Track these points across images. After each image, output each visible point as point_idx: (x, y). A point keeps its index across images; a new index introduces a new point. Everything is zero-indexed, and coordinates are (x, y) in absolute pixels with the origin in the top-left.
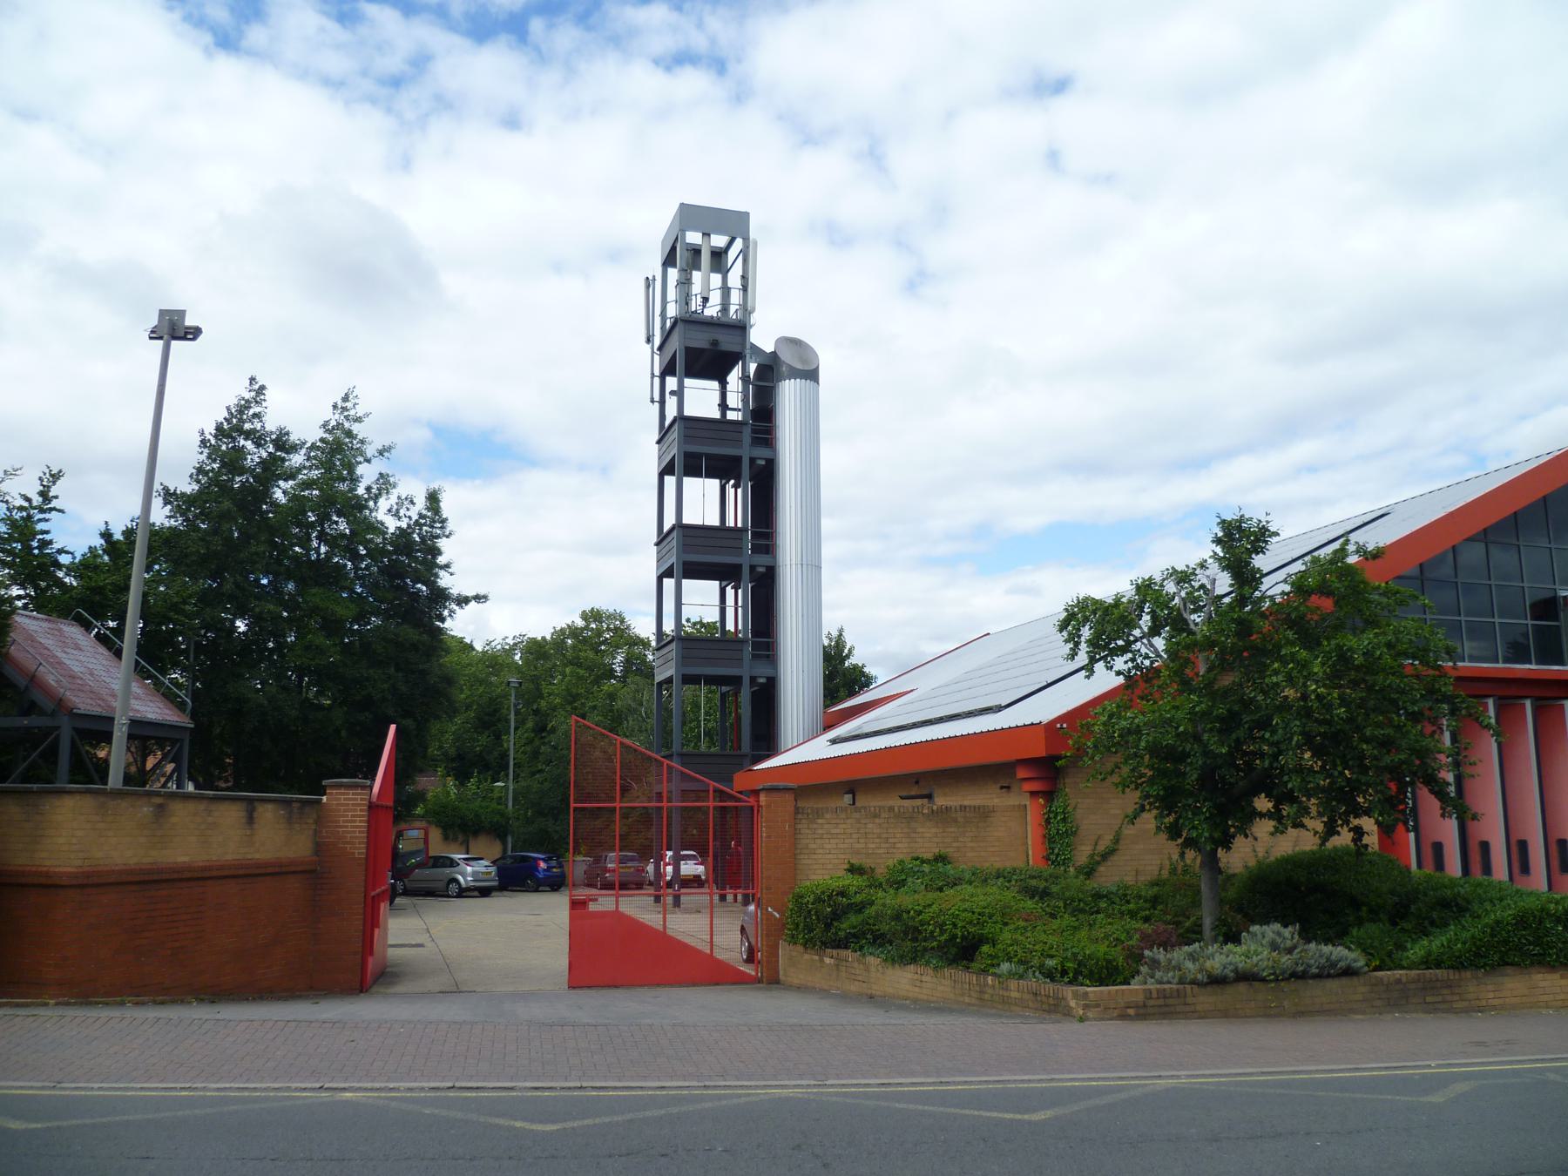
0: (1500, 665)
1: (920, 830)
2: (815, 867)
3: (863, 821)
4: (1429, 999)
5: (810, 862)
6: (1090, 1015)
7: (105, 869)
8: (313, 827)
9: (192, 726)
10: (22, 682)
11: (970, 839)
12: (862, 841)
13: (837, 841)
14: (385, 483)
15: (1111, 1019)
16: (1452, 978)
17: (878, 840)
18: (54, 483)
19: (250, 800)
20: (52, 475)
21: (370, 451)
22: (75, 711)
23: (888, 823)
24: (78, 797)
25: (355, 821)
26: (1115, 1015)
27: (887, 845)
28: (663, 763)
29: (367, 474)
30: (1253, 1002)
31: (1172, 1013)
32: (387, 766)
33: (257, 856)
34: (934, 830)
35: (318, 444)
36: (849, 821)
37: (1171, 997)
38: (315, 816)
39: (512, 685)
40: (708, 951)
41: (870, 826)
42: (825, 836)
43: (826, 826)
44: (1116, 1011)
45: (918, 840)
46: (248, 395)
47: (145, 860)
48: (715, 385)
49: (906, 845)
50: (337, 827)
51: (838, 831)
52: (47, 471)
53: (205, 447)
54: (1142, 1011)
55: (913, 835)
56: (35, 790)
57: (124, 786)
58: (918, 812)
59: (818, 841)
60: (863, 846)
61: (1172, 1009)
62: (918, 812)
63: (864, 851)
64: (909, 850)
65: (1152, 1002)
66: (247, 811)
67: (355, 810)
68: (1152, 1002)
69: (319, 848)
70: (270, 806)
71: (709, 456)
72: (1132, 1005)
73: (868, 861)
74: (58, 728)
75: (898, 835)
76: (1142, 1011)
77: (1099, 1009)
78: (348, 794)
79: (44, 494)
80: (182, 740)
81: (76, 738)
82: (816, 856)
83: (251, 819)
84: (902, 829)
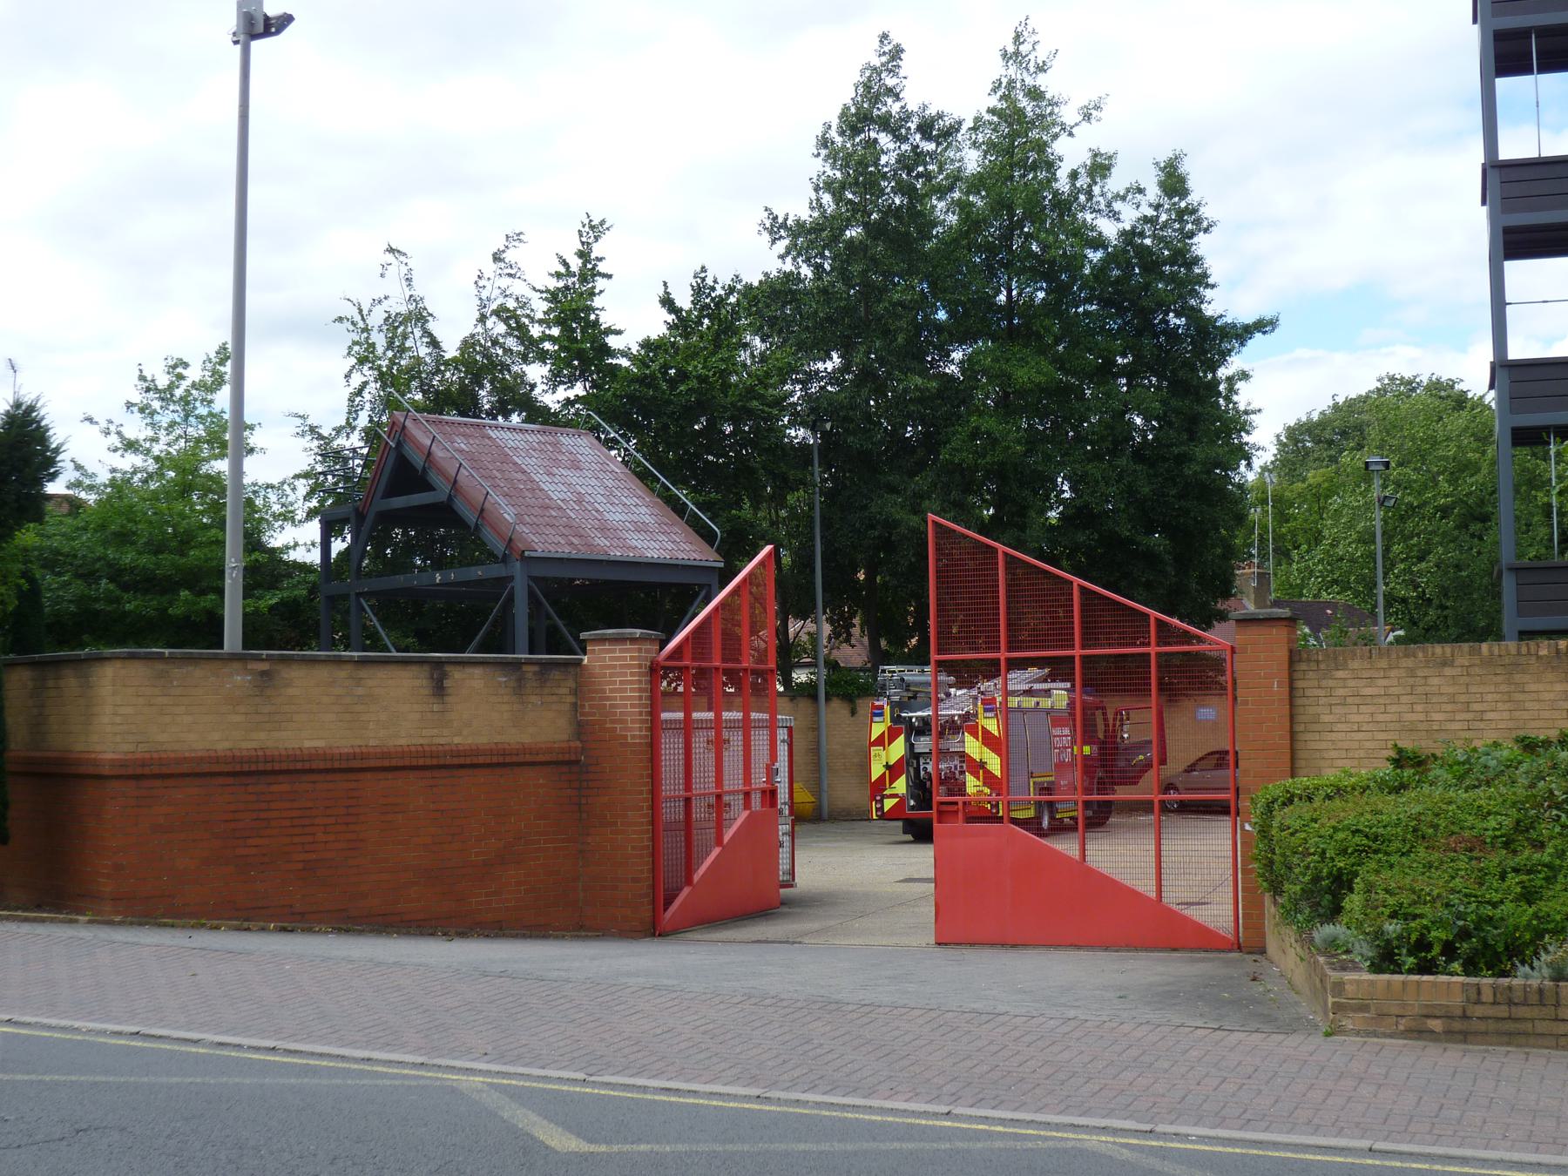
1: (1533, 687)
2: (1334, 754)
5: (1323, 745)
6: (1348, 1023)
7: (173, 755)
8: (571, 699)
9: (722, 565)
10: (471, 517)
12: (1419, 708)
13: (1371, 709)
14: (1100, 167)
15: (1391, 1036)
17: (1449, 707)
18: (597, 239)
19: (439, 663)
20: (592, 227)
21: (1068, 114)
22: (526, 553)
23: (1468, 675)
24: (118, 664)
25: (625, 690)
26: (1401, 1028)
27: (1470, 716)
28: (1072, 582)
29: (1070, 153)
31: (1526, 1034)
33: (457, 740)
34: (1558, 687)
35: (987, 117)
36: (1393, 673)
37: (1525, 1003)
38: (571, 683)
40: (1153, 895)
41: (1436, 681)
42: (1349, 700)
43: (1351, 683)
45: (1528, 705)
46: (876, 62)
47: (245, 745)
49: (1506, 715)
50: (602, 699)
52: (586, 221)
53: (826, 147)
54: (1457, 1025)
56: (264, 657)
57: (245, 647)
58: (1529, 653)
59: (1336, 710)
60: (1422, 717)
62: (1529, 653)
64: (1511, 724)
65: (1479, 1011)
66: (432, 678)
67: (625, 674)
68: (1479, 1011)
69: (581, 729)
70: (478, 671)
73: (1430, 743)
74: (511, 578)
75: (1489, 697)
76: (1457, 1025)
78: (614, 651)
79: (583, 255)
80: (710, 585)
81: (531, 583)
82: (1333, 736)
83: (439, 690)
84: (1496, 684)
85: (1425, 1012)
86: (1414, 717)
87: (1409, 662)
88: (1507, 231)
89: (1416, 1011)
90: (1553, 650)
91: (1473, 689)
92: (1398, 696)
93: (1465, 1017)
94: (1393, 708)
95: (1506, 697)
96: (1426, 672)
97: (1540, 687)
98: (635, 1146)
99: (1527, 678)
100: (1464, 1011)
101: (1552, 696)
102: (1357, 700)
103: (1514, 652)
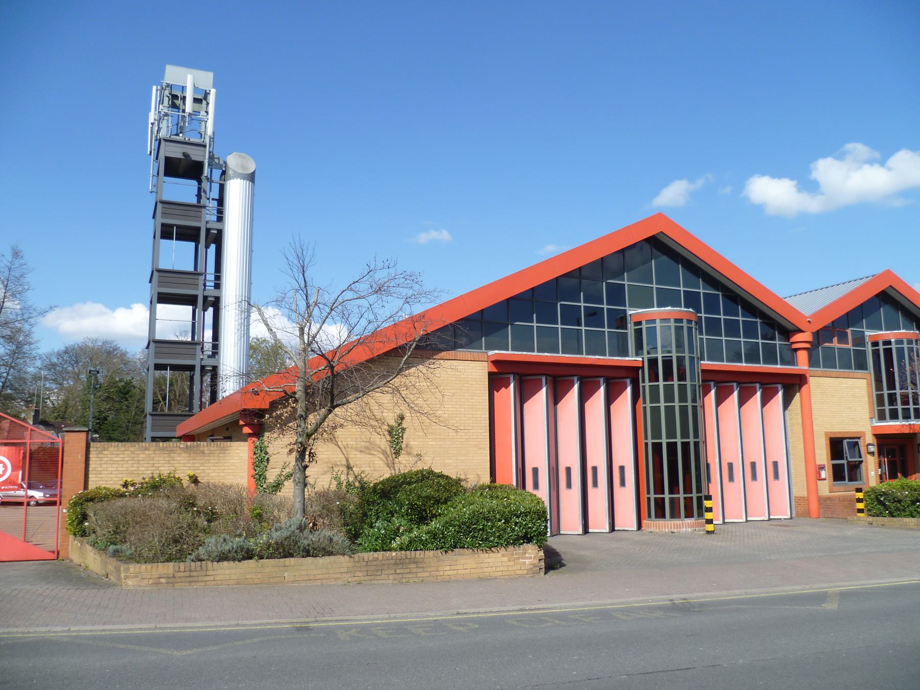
0: (510, 352)
1: (178, 458)
3: (136, 452)
4: (398, 571)
12: (135, 465)
13: (117, 466)
16: (417, 557)
30: (260, 574)
31: (195, 582)
32: (511, 437)
36: (126, 452)
37: (195, 571)
39: (405, 389)
41: (142, 456)
42: (109, 462)
43: (109, 456)
44: (151, 580)
48: (195, 183)
54: (170, 580)
60: (136, 469)
61: (196, 579)
62: (177, 447)
71: (178, 227)
72: (164, 576)
75: (161, 462)
76: (170, 580)
77: (137, 579)
82: (101, 476)
84: (164, 457)
85: (158, 576)
86: (133, 469)
88: (159, 294)
89: (156, 576)
90: (185, 446)
92: (128, 461)
93: (174, 577)
95: (167, 462)
96: (139, 452)
97: (180, 458)
99: (175, 455)
100: (174, 575)
102: (111, 462)
103: (171, 446)
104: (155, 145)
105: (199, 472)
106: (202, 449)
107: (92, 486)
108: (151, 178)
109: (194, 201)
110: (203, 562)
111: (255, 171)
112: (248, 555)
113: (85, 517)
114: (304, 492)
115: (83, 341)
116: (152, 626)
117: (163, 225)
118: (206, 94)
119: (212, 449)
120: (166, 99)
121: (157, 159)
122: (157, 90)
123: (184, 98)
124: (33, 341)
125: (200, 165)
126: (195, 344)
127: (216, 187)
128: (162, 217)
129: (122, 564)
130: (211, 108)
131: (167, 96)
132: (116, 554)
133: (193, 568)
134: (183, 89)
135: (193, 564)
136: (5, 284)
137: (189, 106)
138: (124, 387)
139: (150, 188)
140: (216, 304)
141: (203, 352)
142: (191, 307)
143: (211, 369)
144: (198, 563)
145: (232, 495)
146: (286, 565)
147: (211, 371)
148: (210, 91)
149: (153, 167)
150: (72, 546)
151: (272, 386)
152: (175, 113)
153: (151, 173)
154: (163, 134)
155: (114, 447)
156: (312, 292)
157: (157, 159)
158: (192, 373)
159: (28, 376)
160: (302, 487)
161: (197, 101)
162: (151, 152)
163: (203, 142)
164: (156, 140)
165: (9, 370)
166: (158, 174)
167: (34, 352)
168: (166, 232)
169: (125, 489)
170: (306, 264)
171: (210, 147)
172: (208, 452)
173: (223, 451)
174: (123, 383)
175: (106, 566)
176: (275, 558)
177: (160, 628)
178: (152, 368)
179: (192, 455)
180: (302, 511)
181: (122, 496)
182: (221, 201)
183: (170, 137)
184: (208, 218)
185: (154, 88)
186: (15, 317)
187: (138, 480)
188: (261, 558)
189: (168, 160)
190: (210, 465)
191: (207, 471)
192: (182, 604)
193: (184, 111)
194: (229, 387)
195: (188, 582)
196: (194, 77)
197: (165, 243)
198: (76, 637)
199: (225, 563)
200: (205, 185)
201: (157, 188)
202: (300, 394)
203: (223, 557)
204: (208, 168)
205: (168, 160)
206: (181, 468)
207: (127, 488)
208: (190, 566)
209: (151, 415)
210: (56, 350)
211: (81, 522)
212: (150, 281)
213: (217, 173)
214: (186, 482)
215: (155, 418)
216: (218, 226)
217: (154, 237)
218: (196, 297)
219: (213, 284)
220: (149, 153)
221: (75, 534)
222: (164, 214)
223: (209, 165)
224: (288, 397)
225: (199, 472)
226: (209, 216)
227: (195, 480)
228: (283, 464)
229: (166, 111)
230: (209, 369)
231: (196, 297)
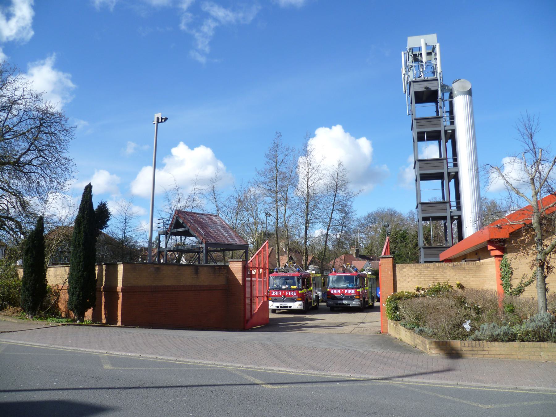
1: (448, 273)
3: (422, 270)
11: (472, 277)
12: (422, 278)
13: (411, 278)
27: (434, 280)
31: (476, 354)
36: (416, 270)
37: (476, 347)
41: (426, 272)
42: (407, 276)
51: (412, 274)
55: (445, 275)
58: (447, 265)
60: (423, 280)
61: (476, 352)
62: (447, 265)
63: (424, 282)
71: (428, 132)
82: (403, 284)
86: (421, 280)
87: (420, 267)
88: (421, 174)
91: (435, 273)
94: (417, 278)
96: (424, 270)
98: (487, 407)
99: (447, 271)
101: (453, 275)
102: (408, 276)
104: (407, 87)
105: (463, 281)
106: (463, 267)
107: (399, 291)
108: (407, 106)
109: (434, 115)
110: (480, 341)
111: (471, 88)
112: (512, 338)
113: (397, 309)
114: (545, 294)
115: (377, 209)
116: (455, 382)
117: (418, 133)
118: (434, 48)
119: (470, 266)
120: (410, 57)
121: (409, 94)
122: (404, 54)
123: (421, 54)
124: (353, 211)
125: (436, 92)
126: (445, 203)
127: (447, 104)
128: (417, 128)
129: (426, 339)
130: (438, 56)
131: (411, 55)
132: (421, 332)
133: (474, 345)
134: (420, 48)
135: (474, 342)
136: (336, 181)
137: (424, 59)
138: (403, 234)
139: (408, 113)
140: (456, 177)
141: (450, 208)
142: (440, 180)
143: (457, 217)
144: (477, 342)
145: (489, 297)
146: (541, 347)
147: (457, 219)
148: (436, 45)
149: (407, 99)
150: (390, 326)
151: (514, 221)
152: (417, 64)
153: (407, 104)
154: (412, 78)
155: (409, 266)
156: (538, 151)
157: (409, 94)
158: (445, 221)
159: (351, 230)
160: (544, 291)
161: (429, 54)
162: (405, 92)
163: (436, 77)
164: (408, 84)
165: (342, 228)
166: (411, 103)
167: (354, 217)
168: (421, 137)
169: (418, 292)
170: (533, 131)
171: (440, 80)
172: (468, 268)
173: (477, 268)
174: (402, 232)
175: (415, 340)
176: (533, 341)
177: (462, 385)
178: (421, 219)
179: (457, 271)
180: (545, 308)
181: (417, 296)
182: (451, 112)
183: (416, 79)
184: (445, 123)
185: (403, 53)
186: (343, 198)
187: (425, 286)
188: (523, 341)
189: (416, 93)
190: (469, 277)
191: (468, 281)
192: (471, 370)
193: (422, 62)
194: (469, 230)
195: (471, 354)
196: (425, 40)
197: (421, 143)
198: (408, 385)
199: (496, 343)
200: (440, 103)
201: (412, 112)
202: (535, 225)
203: (494, 339)
204: (441, 93)
205: (416, 93)
206: (452, 279)
207: (419, 291)
208: (472, 343)
209: (424, 248)
210: (363, 216)
211: (395, 312)
212: (414, 168)
213: (447, 95)
214: (455, 287)
215: (426, 250)
216: (452, 127)
217: (414, 141)
218: (443, 174)
219: (452, 164)
220: (404, 92)
221: (392, 319)
222: (418, 126)
223: (441, 91)
224: (528, 227)
225: (463, 281)
226: (445, 122)
227: (461, 287)
228: (522, 275)
229: (412, 65)
230: (456, 217)
231: (443, 174)
